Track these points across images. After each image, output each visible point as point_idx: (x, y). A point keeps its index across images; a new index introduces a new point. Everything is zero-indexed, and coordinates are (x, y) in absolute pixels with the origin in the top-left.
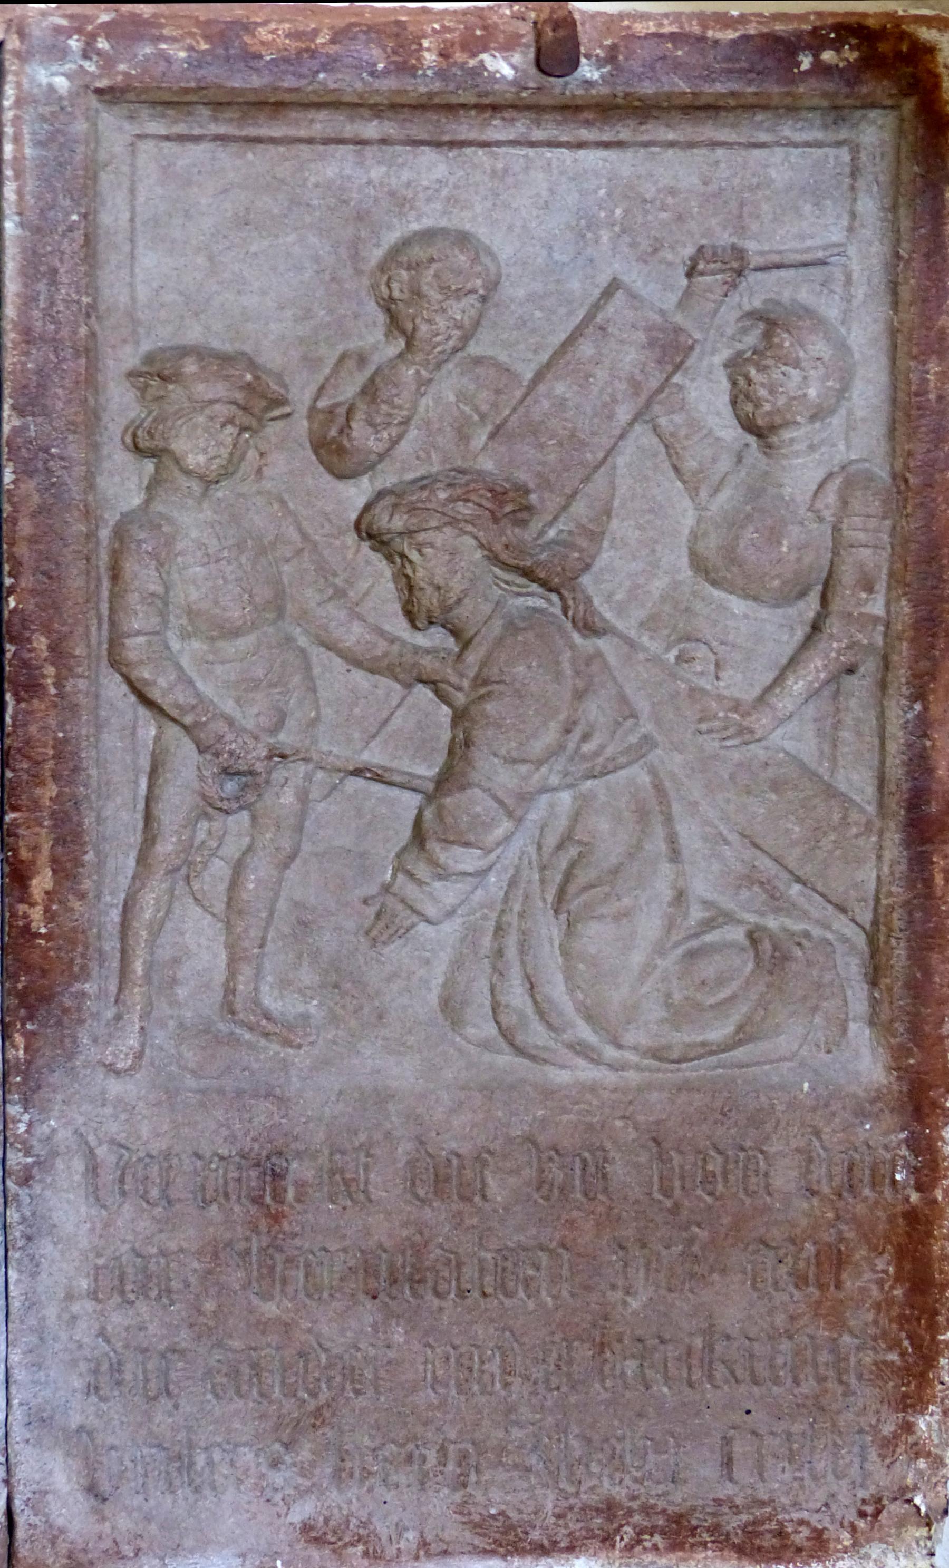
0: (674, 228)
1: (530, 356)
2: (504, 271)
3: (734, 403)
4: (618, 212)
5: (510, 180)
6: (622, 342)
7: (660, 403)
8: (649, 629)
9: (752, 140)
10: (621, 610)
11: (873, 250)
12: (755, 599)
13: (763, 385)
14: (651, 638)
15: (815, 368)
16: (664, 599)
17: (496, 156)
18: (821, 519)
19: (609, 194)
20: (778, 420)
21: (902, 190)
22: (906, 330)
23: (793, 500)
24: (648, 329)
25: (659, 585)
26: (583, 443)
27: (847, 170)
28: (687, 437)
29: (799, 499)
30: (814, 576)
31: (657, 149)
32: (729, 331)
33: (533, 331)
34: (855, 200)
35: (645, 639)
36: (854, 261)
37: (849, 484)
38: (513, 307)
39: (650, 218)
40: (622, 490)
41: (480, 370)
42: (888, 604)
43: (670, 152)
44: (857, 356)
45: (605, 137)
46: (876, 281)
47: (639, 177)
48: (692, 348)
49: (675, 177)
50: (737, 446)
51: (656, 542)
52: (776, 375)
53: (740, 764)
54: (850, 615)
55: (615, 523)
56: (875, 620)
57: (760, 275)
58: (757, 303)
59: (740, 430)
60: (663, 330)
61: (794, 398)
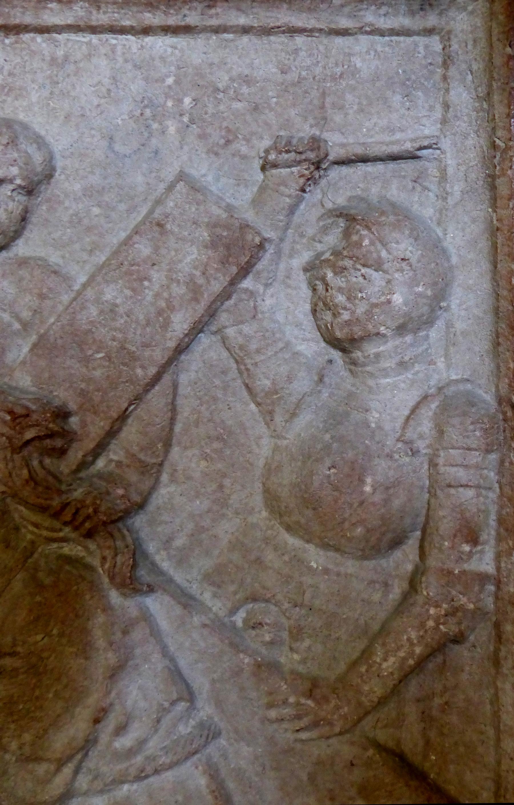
0: (248, 117)
1: (85, 256)
2: (59, 163)
3: (314, 311)
4: (187, 101)
5: (71, 68)
6: (183, 239)
7: (227, 311)
8: (213, 584)
9: (333, 26)
10: (182, 560)
11: (470, 142)
12: (337, 550)
13: (340, 290)
14: (215, 595)
15: (401, 270)
16: (233, 546)
17: (56, 44)
18: (415, 453)
19: (177, 82)
20: (358, 332)
21: (495, 75)
22: (505, 228)
23: (380, 428)
24: (213, 225)
25: (226, 529)
26: (133, 358)
27: (440, 60)
28: (258, 351)
29: (387, 427)
30: (408, 521)
31: (231, 36)
32: (310, 232)
33: (89, 229)
34: (447, 90)
35: (207, 597)
36: (448, 155)
37: (445, 408)
38: (67, 204)
39: (222, 107)
40: (185, 412)
41: (24, 273)
42: (498, 557)
43: (245, 39)
44: (454, 260)
45: (172, 21)
46: (473, 176)
47: (211, 64)
48: (261, 246)
49: (251, 66)
50: (322, 360)
51: (224, 476)
52: (356, 279)
53: (319, 763)
54: (450, 573)
55: (175, 451)
56: (483, 578)
57: (344, 170)
58: (341, 201)
59: (323, 344)
60: (227, 227)
61: (376, 305)
